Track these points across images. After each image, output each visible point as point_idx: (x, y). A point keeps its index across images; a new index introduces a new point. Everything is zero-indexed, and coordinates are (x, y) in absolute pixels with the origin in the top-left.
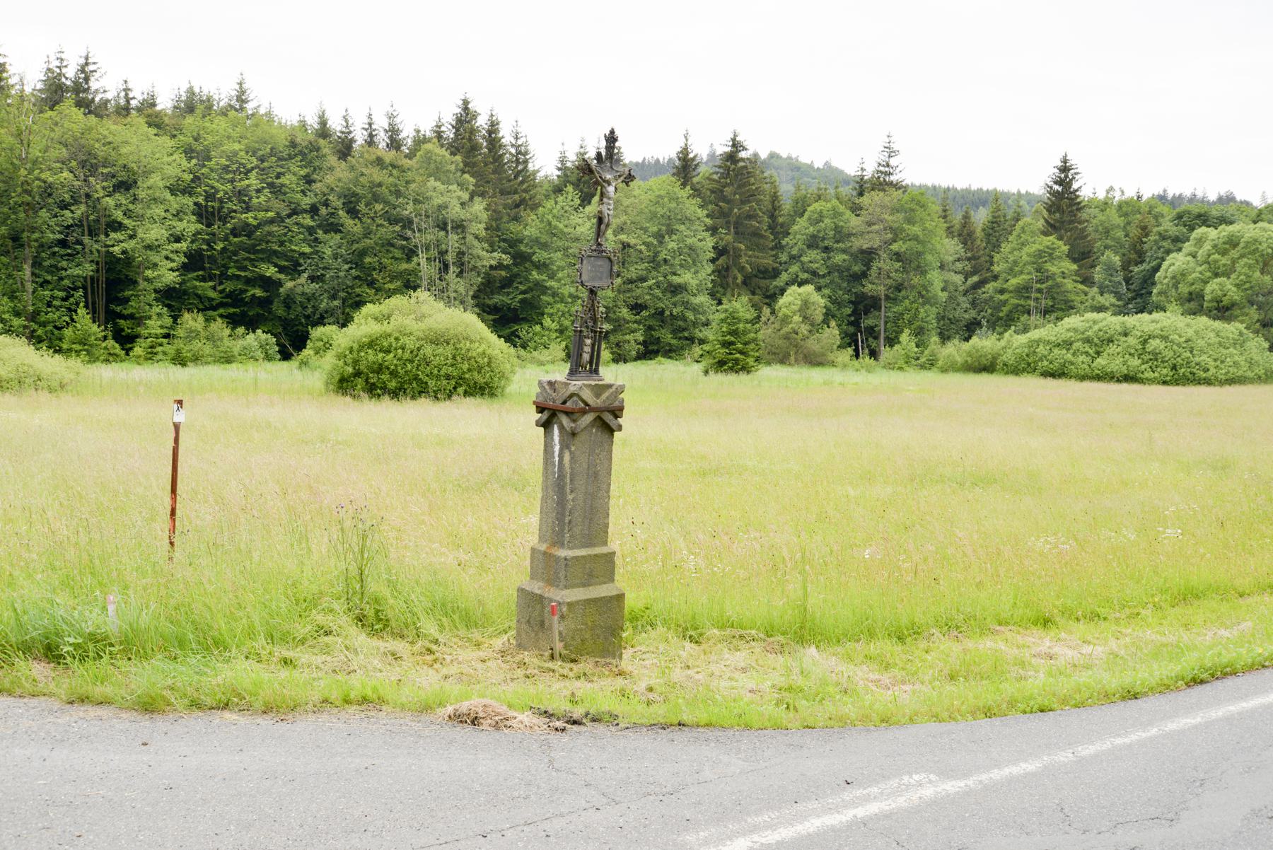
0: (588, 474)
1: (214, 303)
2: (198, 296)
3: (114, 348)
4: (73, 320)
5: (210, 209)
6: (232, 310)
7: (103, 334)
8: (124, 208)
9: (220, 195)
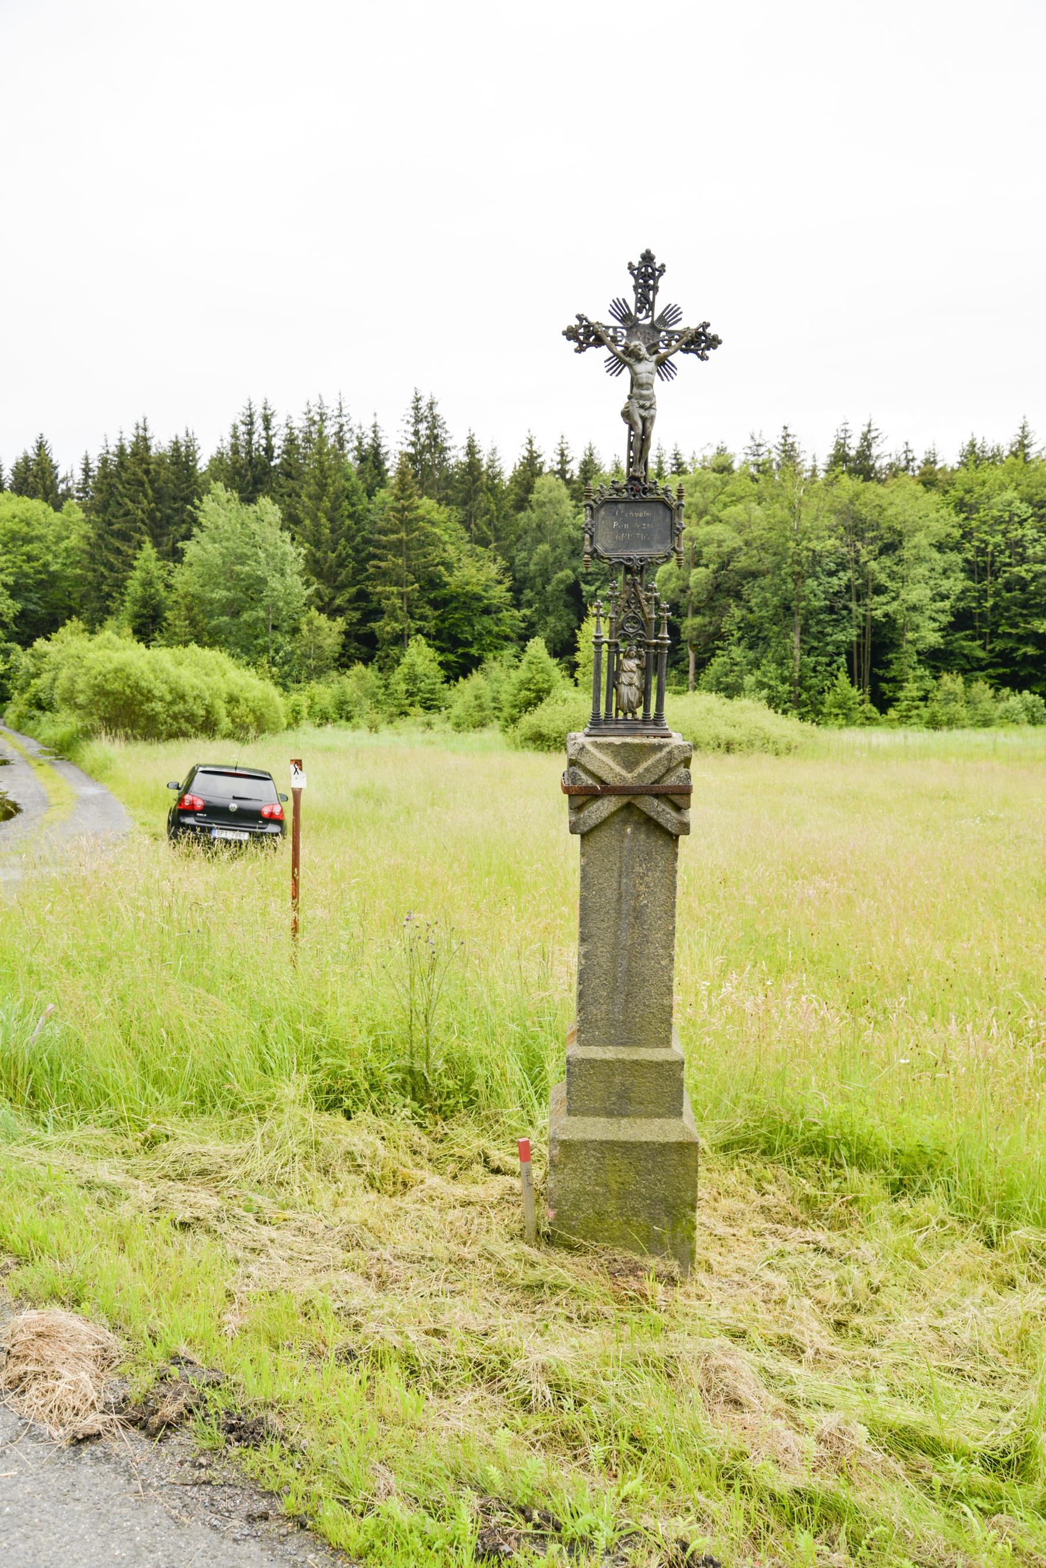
0: (619, 911)
1: (983, 663)
2: (965, 656)
3: (870, 711)
4: (834, 685)
5: (982, 565)
6: (1001, 671)
7: (862, 697)
8: (888, 571)
9: (990, 548)
